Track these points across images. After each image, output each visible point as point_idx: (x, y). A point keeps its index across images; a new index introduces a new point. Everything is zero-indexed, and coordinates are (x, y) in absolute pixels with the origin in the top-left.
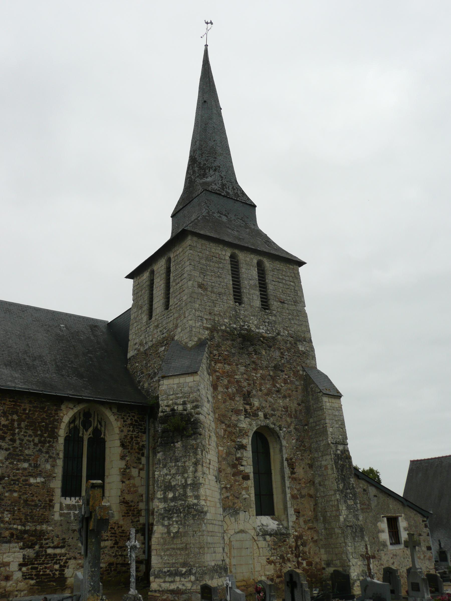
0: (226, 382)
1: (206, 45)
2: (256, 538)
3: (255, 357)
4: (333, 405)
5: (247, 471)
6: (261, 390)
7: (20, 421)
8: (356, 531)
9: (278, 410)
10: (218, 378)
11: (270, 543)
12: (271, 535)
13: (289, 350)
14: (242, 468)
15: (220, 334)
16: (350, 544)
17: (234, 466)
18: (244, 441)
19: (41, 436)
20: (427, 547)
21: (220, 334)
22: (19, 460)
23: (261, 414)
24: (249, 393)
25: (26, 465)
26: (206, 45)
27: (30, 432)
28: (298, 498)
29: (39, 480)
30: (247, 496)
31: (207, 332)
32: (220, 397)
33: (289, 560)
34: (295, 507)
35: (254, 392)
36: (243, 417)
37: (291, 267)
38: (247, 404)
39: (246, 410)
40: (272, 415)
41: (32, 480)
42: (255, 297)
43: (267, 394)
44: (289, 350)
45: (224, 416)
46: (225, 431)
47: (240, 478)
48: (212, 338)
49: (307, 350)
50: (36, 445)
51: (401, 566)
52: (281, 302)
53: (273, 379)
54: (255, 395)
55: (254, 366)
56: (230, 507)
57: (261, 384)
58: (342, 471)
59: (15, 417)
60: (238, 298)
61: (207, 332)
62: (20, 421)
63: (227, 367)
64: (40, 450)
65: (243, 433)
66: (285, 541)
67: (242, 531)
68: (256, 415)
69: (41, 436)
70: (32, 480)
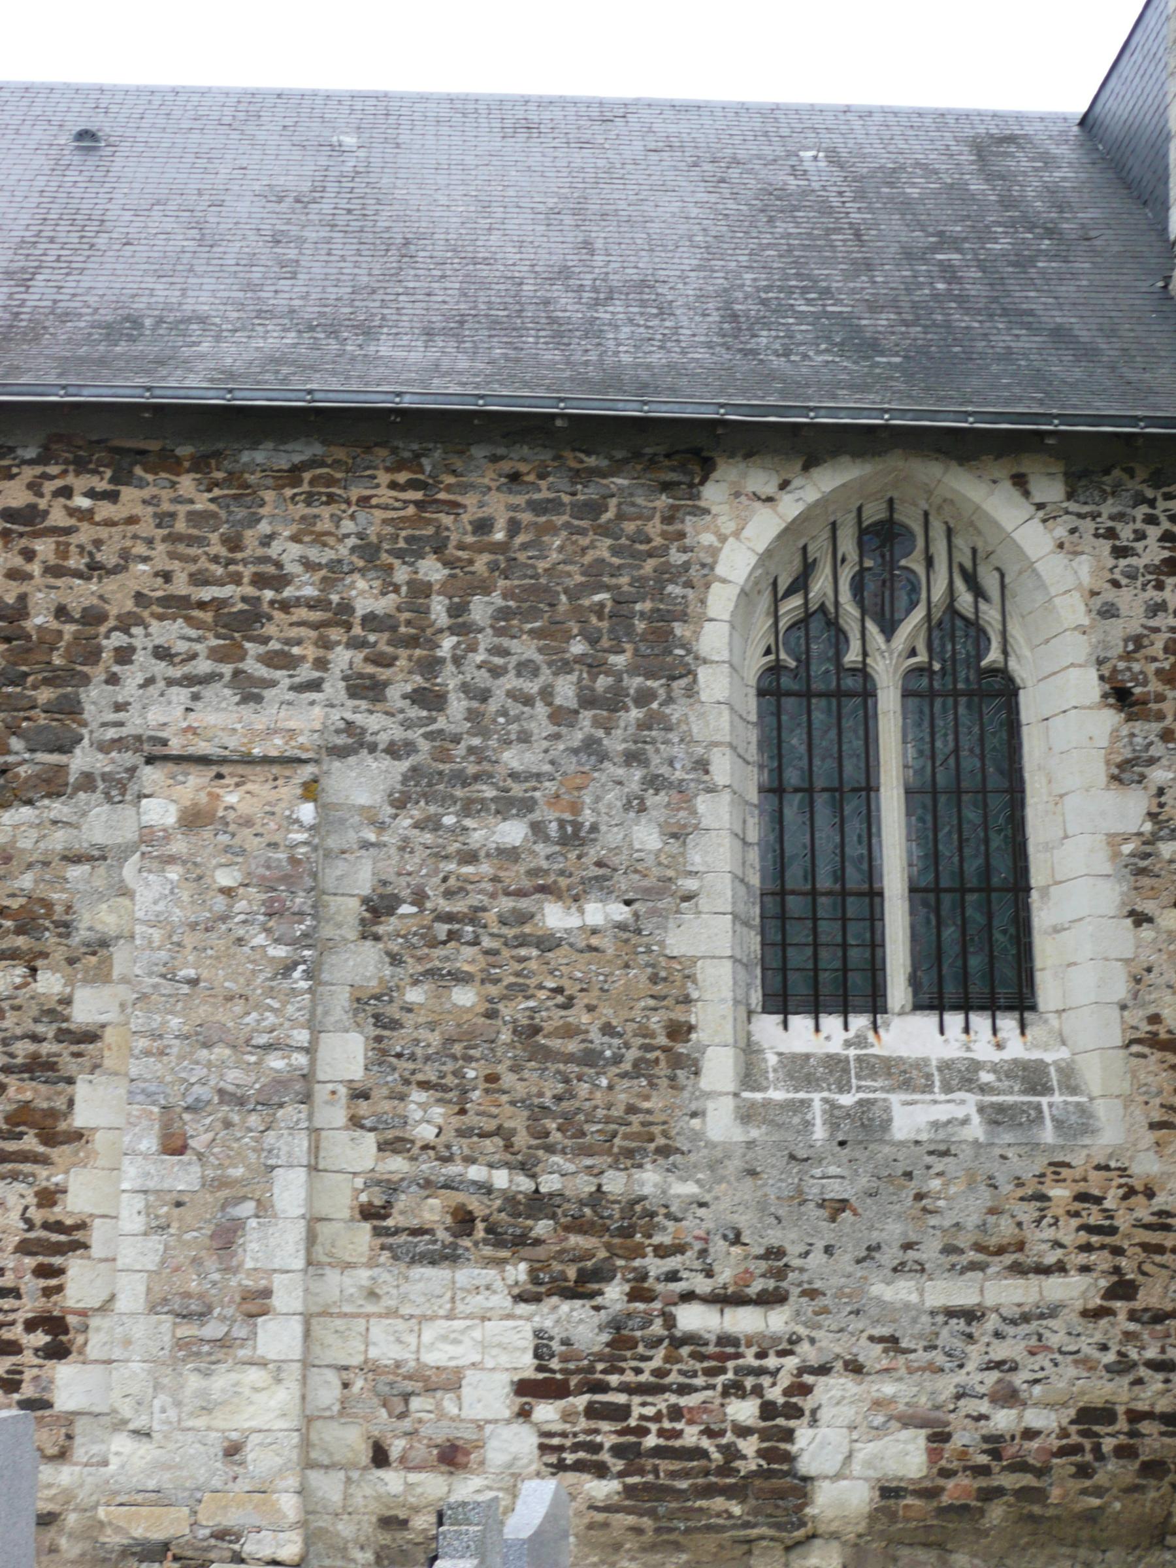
1: (942, 1032)
25: (513, 832)
26: (942, 1032)
27: (525, 648)
29: (600, 912)
41: (555, 917)
50: (561, 717)
69: (595, 667)
70: (555, 917)
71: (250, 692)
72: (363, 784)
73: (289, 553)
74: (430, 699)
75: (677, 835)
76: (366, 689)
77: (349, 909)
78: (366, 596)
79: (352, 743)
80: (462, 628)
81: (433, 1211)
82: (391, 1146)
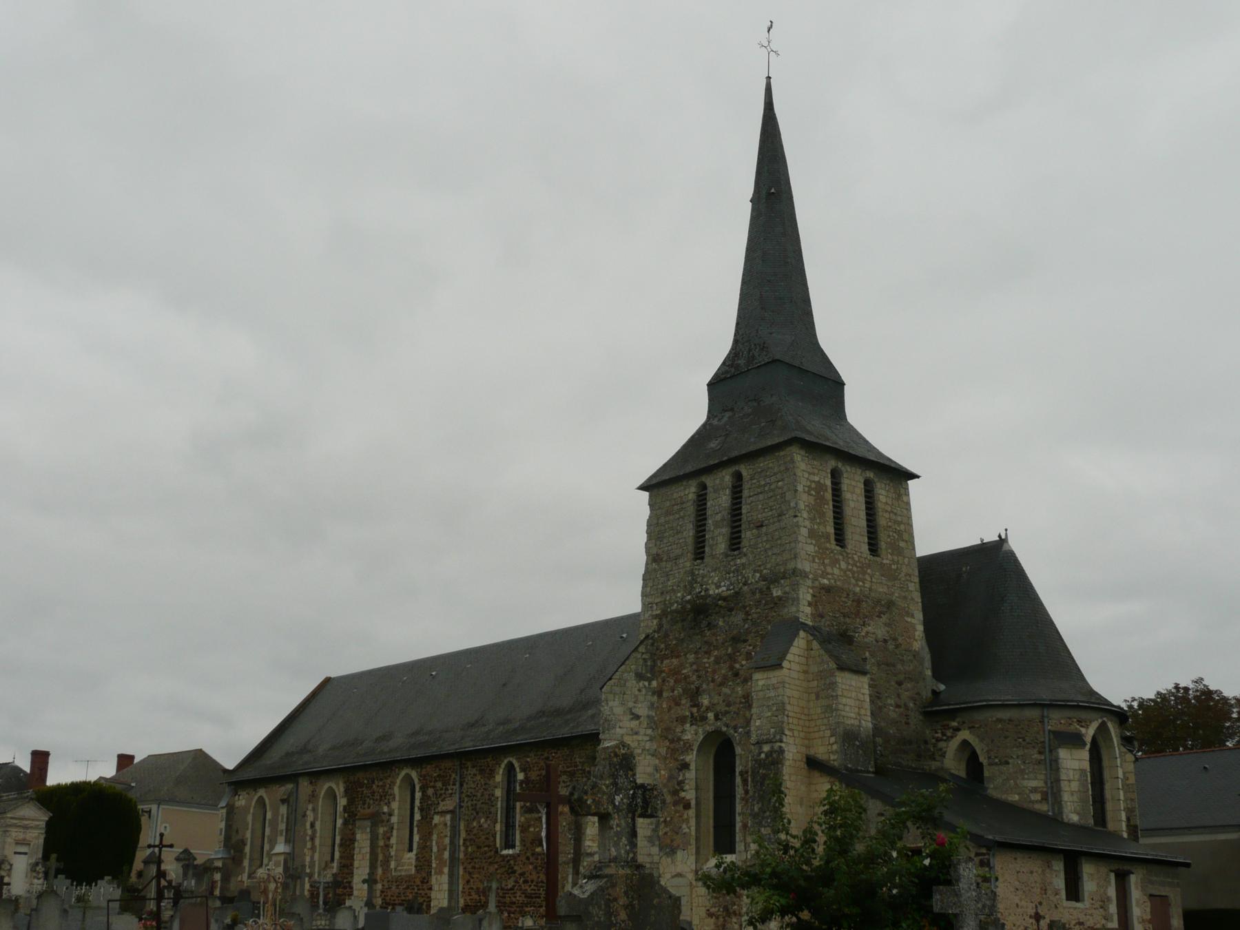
1: (769, 78)
6: (713, 681)
14: (683, 794)
23: (711, 715)
26: (769, 78)
35: (704, 686)
37: (782, 453)
40: (727, 712)
42: (720, 539)
43: (722, 684)
45: (668, 729)
47: (680, 808)
48: (660, 626)
49: (785, 593)
53: (732, 658)
55: (705, 648)
60: (699, 554)
61: (655, 622)
63: (675, 661)
65: (688, 747)
67: (679, 875)
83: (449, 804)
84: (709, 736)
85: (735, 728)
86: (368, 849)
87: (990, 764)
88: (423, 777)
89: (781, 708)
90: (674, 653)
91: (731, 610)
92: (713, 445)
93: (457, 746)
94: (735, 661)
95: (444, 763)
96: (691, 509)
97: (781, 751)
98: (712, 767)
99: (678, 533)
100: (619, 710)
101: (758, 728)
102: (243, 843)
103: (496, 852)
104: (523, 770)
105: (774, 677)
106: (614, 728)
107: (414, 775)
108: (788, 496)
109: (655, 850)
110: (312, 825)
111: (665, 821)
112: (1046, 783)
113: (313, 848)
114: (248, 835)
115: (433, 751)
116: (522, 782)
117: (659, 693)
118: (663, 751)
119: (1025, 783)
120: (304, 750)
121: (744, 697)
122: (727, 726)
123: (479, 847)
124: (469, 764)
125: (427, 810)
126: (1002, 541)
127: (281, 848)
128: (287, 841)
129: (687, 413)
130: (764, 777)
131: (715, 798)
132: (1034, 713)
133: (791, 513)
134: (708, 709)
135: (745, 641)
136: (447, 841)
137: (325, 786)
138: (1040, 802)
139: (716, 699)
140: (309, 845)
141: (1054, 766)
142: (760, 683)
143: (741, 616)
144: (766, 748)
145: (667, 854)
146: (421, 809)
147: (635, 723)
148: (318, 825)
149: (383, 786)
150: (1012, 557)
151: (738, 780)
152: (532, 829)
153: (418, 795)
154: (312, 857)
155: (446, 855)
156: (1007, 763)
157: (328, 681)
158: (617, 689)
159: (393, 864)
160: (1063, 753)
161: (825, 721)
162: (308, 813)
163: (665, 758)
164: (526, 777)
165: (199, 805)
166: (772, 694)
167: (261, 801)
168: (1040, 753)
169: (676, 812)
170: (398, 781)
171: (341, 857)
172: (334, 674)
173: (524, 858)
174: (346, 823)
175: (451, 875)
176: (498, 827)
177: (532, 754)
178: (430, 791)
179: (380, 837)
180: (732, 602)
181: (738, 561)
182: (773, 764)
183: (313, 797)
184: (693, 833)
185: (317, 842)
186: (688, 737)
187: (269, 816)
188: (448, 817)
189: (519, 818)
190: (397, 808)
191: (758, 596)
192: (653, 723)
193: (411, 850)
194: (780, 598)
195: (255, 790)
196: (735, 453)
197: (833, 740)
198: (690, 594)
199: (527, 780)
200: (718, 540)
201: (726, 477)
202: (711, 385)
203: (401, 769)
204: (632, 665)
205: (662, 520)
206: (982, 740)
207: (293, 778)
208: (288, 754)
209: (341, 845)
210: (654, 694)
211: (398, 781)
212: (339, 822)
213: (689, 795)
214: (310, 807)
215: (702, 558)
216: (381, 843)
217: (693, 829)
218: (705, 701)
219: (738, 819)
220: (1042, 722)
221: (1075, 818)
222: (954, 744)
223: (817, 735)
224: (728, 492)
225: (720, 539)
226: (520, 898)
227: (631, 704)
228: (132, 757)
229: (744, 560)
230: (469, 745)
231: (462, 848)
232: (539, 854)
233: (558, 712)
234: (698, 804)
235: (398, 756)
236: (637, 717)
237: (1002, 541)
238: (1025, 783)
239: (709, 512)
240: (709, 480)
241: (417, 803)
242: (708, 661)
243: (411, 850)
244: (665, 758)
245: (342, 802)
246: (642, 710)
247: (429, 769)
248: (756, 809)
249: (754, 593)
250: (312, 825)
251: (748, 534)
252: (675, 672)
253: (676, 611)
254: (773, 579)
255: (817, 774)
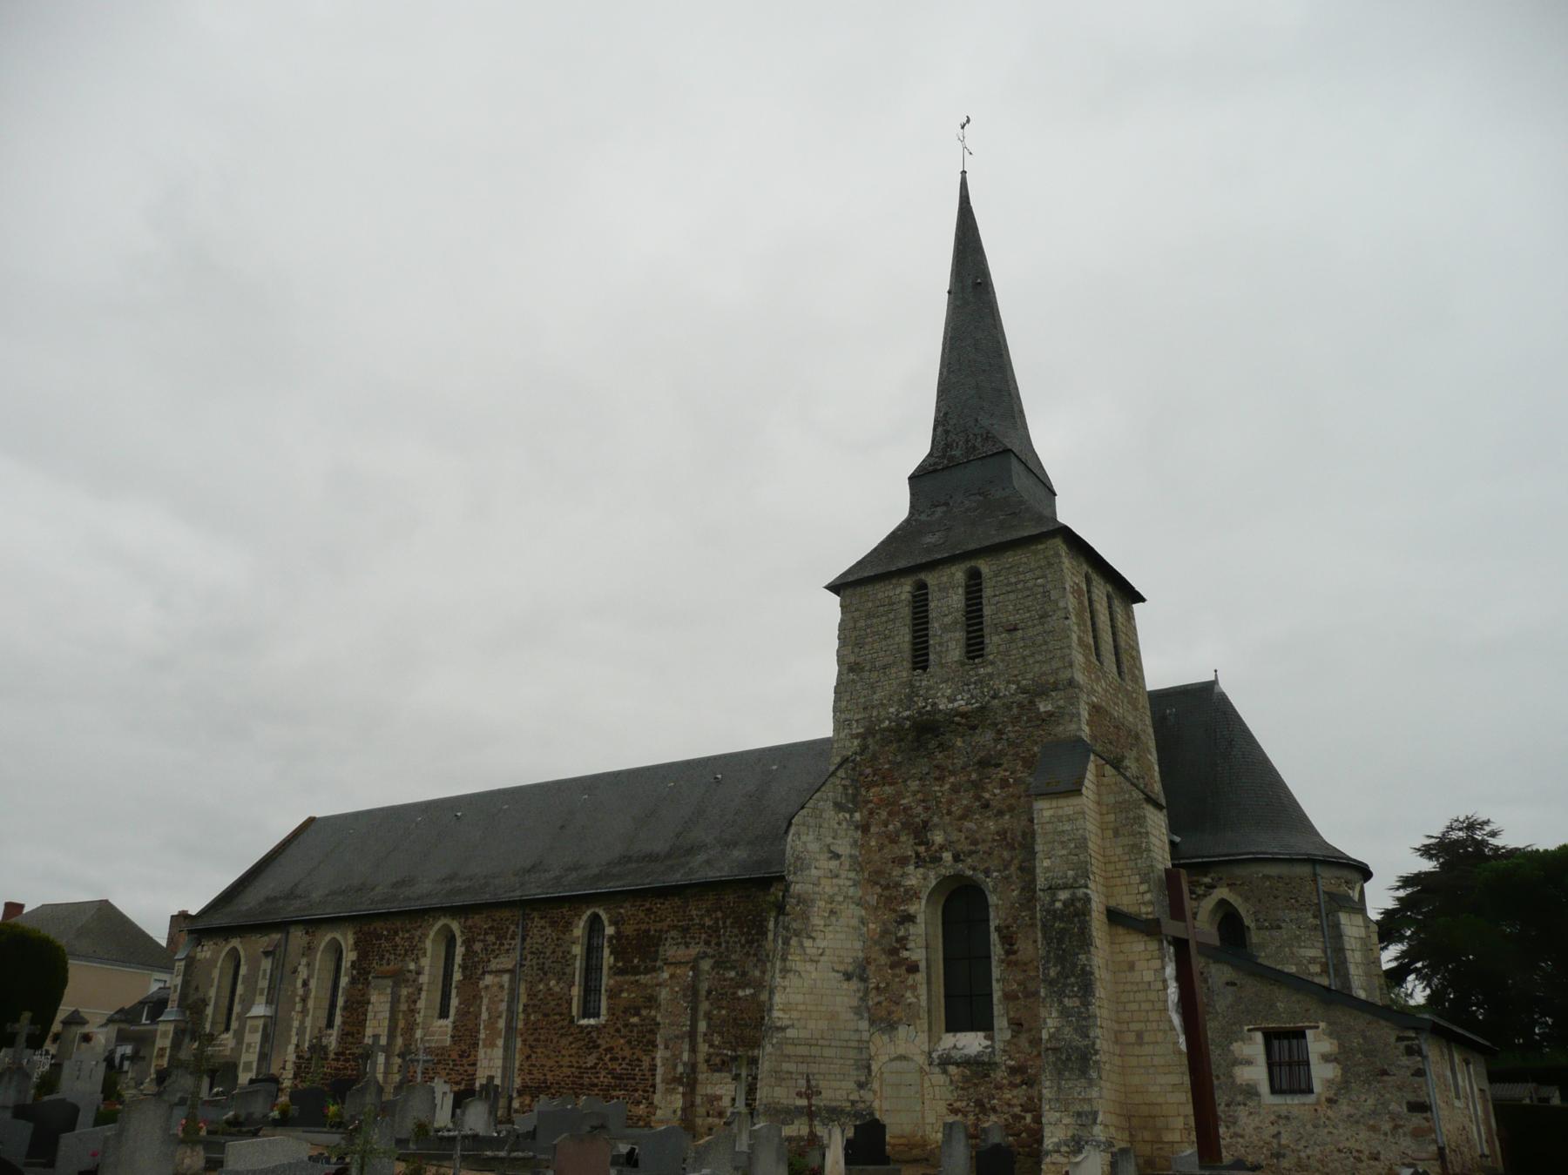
0: (884, 815)
1: (964, 172)
2: (927, 1068)
3: (940, 756)
4: (1060, 812)
5: (914, 958)
6: (949, 813)
7: (724, 919)
8: (1069, 1059)
9: (984, 841)
10: (871, 813)
11: (955, 1078)
12: (958, 1065)
13: (1016, 720)
14: (905, 954)
15: (878, 737)
16: (1048, 1083)
17: (893, 952)
18: (912, 909)
19: (749, 933)
20: (1409, 1103)
21: (878, 737)
22: (726, 969)
24: (925, 823)
25: (733, 974)
26: (964, 172)
27: (736, 931)
28: (1017, 998)
29: (748, 991)
30: (914, 1000)
31: (856, 742)
32: (873, 843)
33: (994, 1110)
34: (1012, 1014)
35: (936, 819)
36: (912, 867)
37: (1040, 547)
38: (920, 844)
39: (918, 855)
40: (971, 853)
41: (740, 993)
42: (952, 645)
43: (963, 817)
44: (1016, 720)
45: (879, 872)
46: (880, 896)
48: (864, 748)
50: (743, 946)
51: (1303, 1143)
52: (1009, 631)
53: (978, 786)
54: (936, 825)
55: (937, 773)
56: (882, 1020)
57: (950, 802)
58: (1060, 941)
59: (719, 914)
60: (920, 660)
61: (856, 742)
62: (724, 919)
63: (888, 789)
64: (748, 954)
66: (987, 1075)
68: (936, 860)
69: (749, 933)
70: (740, 993)
71: (687, 945)
72: (706, 965)
73: (694, 913)
74: (719, 944)
75: (764, 972)
76: (707, 943)
77: (703, 993)
78: (708, 922)
79: (705, 956)
80: (725, 927)
81: (718, 1060)
82: (711, 1046)
83: (506, 962)
84: (944, 881)
85: (987, 872)
86: (388, 1015)
87: (1259, 928)
88: (466, 929)
89: (1082, 844)
90: (886, 779)
91: (974, 728)
92: (930, 539)
93: (518, 893)
94: (984, 789)
95: (491, 915)
96: (906, 612)
97: (1087, 899)
98: (940, 922)
99: (886, 638)
100: (814, 847)
101: (1048, 869)
102: (205, 1003)
103: (572, 1021)
104: (612, 923)
105: (1068, 806)
106: (809, 868)
107: (455, 926)
108: (1054, 595)
109: (864, 1025)
110: (305, 984)
111: (877, 988)
112: (1325, 952)
113: (304, 1011)
114: (212, 993)
115: (487, 897)
116: (611, 938)
117: (865, 828)
118: (873, 900)
119: (1303, 952)
120: (291, 895)
121: (998, 833)
122: (974, 869)
123: (546, 1015)
124: (535, 914)
125: (473, 970)
126: (1214, 683)
127: (259, 1009)
128: (269, 1002)
129: (891, 508)
130: (1063, 932)
131: (945, 959)
132: (1304, 870)
133: (1061, 614)
134: (942, 848)
135: (998, 765)
136: (503, 1006)
137: (326, 937)
138: (1320, 975)
139: (954, 836)
140: (298, 1007)
141: (1336, 934)
142: (1047, 814)
143: (990, 735)
144: (1064, 895)
145: (882, 1031)
146: (464, 967)
147: (834, 864)
148: (313, 984)
149: (411, 939)
150: (1224, 699)
151: (994, 937)
152: (625, 995)
153: (460, 950)
154: (302, 1023)
155: (501, 1024)
156: (1279, 927)
157: (311, 820)
158: (811, 821)
159: (419, 1034)
160: (1344, 918)
161: (1131, 864)
162: (300, 968)
163: (876, 908)
164: (618, 932)
165: (101, 960)
166: (1067, 827)
167: (234, 956)
168: (1315, 917)
169: (895, 976)
170: (432, 934)
171: (344, 1023)
172: (319, 814)
173: (612, 1031)
174: (353, 981)
175: (506, 1048)
176: (575, 991)
177: (627, 905)
178: (478, 946)
179: (403, 999)
180: (971, 721)
181: (982, 671)
182: (1076, 915)
183: (309, 950)
184: (924, 1003)
185: (311, 1004)
186: (912, 881)
187: (243, 970)
188: (506, 978)
189: (606, 981)
190: (428, 965)
191: (1015, 711)
192: (856, 865)
193: (444, 1014)
194: (1050, 714)
195: (226, 940)
196: (972, 546)
197: (1143, 888)
198: (909, 708)
199: (618, 935)
200: (949, 645)
201: (958, 573)
202: (914, 479)
203: (436, 919)
204: (831, 792)
205: (862, 623)
206: (1247, 899)
207: (283, 926)
208: (268, 900)
209: (345, 1008)
210: (857, 828)
211: (432, 934)
212: (344, 981)
213: (917, 954)
214: (304, 961)
215: (925, 668)
216: (404, 1007)
217: (924, 998)
218: (938, 838)
219: (996, 986)
220: (1315, 881)
221: (1362, 995)
222: (1209, 903)
223: (1118, 881)
224: (961, 591)
225: (952, 645)
226: (604, 1078)
227: (829, 840)
228: (21, 906)
229: (989, 670)
230: (535, 892)
231: (522, 1016)
232: (635, 1025)
233: (652, 858)
234: (928, 967)
235: (434, 902)
236: (837, 856)
237: (1214, 683)
238: (1303, 952)
239: (932, 615)
240: (931, 579)
241: (458, 960)
242: (942, 790)
243: (444, 1014)
244: (876, 908)
245: (350, 956)
246: (843, 848)
247: (477, 920)
248: (1052, 973)
249: (1009, 708)
250: (305, 984)
251: (995, 639)
252: (890, 803)
253: (889, 729)
254: (1041, 690)
255: (1121, 931)
